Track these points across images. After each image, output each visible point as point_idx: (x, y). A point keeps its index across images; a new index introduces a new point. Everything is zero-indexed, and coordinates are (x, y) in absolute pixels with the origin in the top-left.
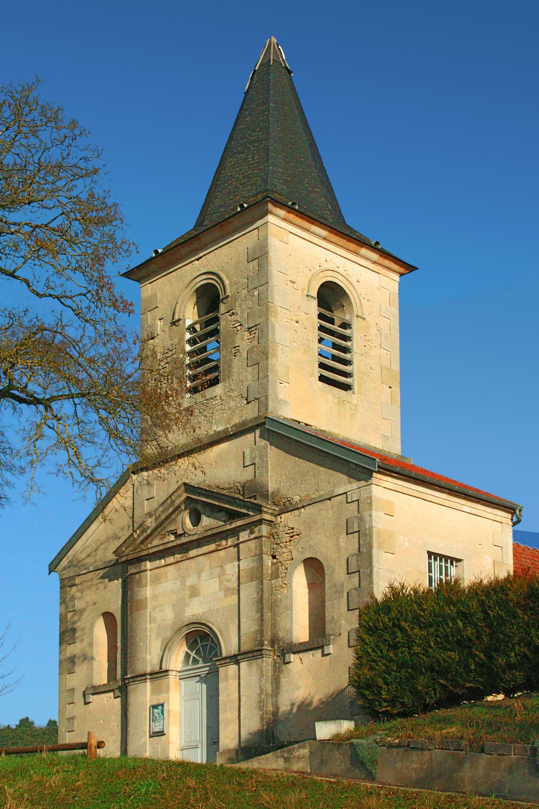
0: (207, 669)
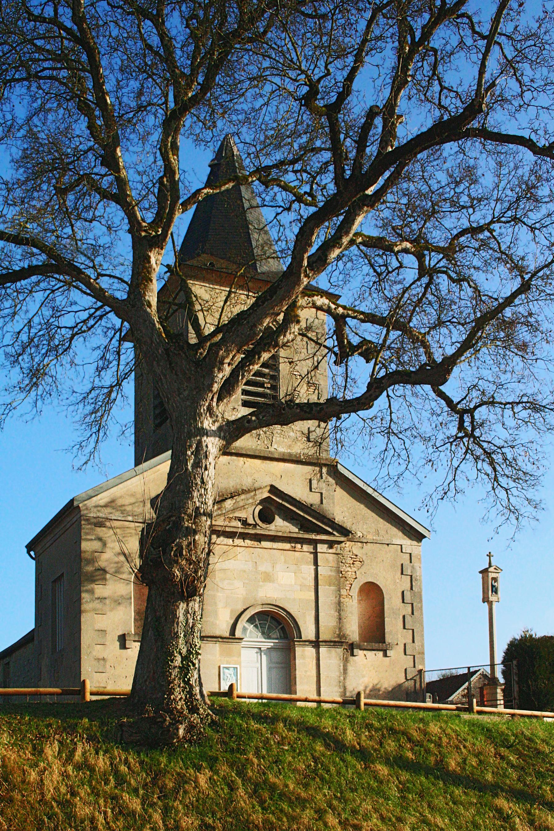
0: (272, 644)
